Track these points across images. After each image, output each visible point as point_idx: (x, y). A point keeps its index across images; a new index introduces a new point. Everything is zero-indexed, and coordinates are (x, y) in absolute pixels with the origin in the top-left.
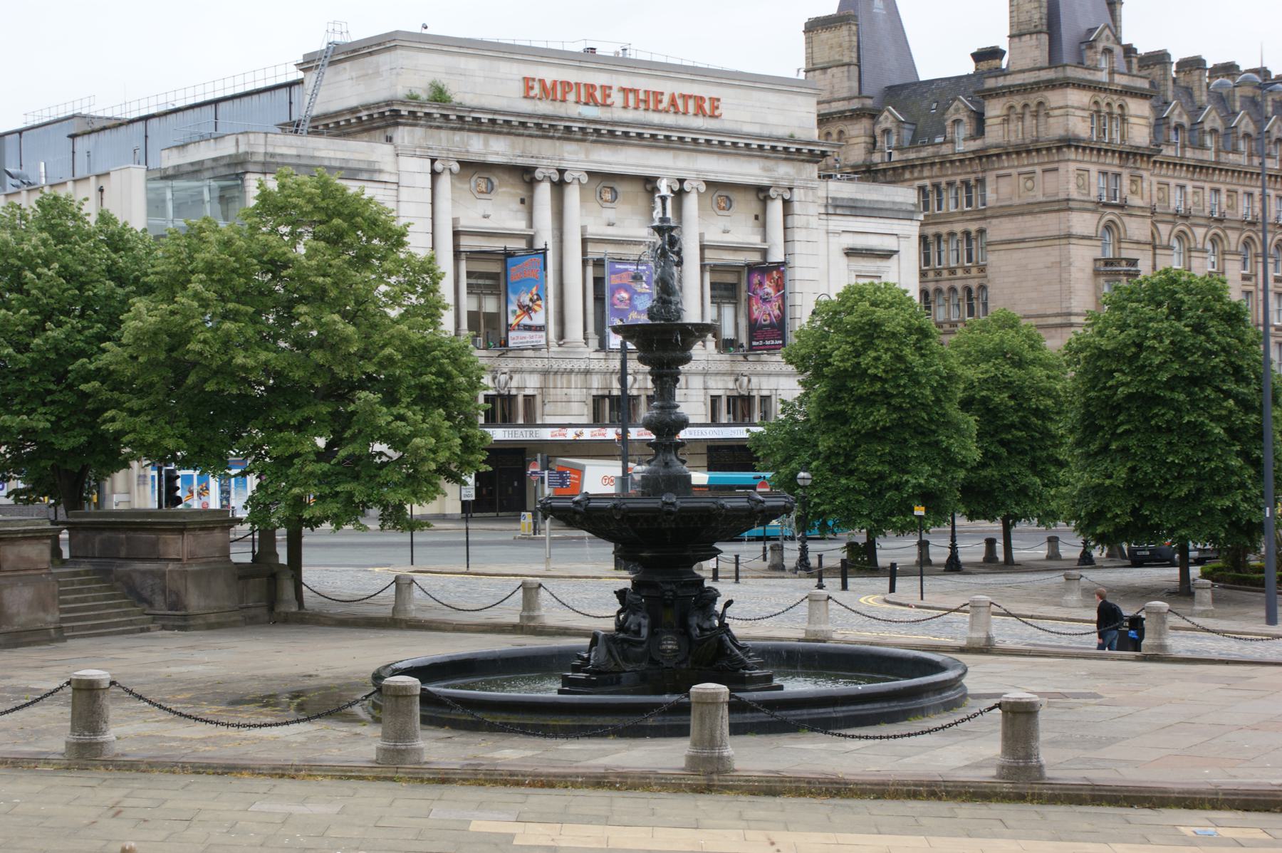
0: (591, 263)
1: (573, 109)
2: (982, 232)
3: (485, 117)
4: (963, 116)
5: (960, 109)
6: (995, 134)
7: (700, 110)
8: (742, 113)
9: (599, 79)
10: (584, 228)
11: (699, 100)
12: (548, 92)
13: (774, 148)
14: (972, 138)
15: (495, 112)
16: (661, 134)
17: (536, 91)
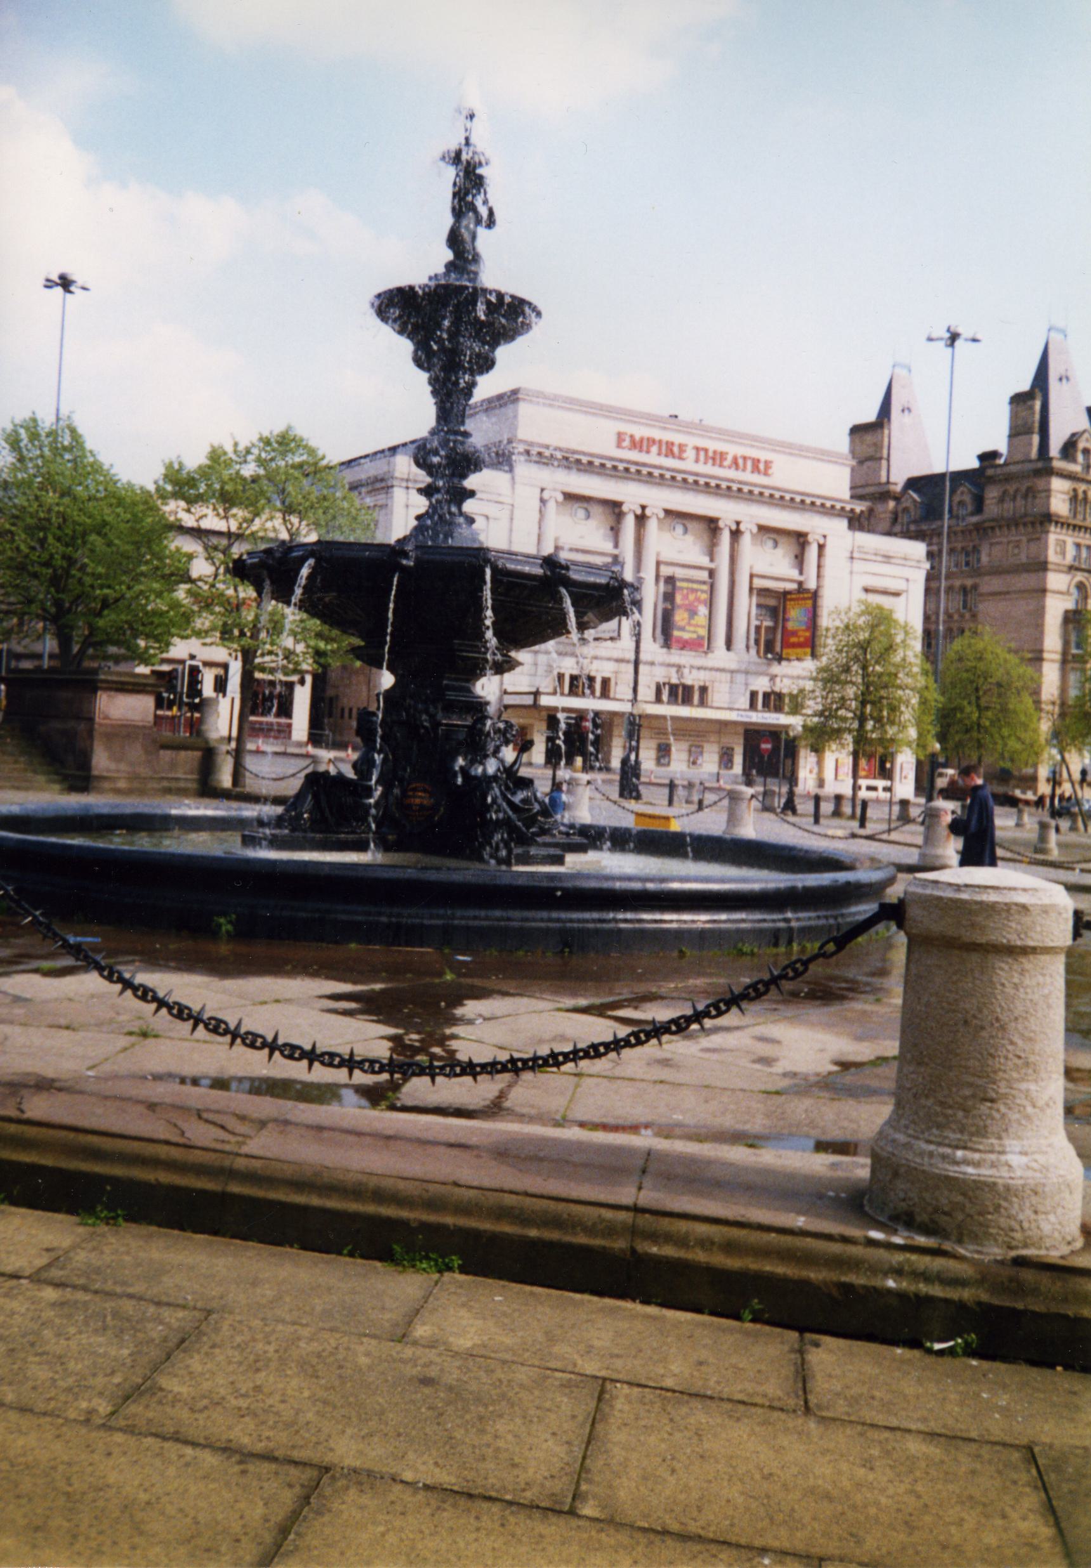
1: (653, 458)
2: (975, 587)
3: (585, 459)
4: (967, 498)
5: (965, 494)
6: (992, 508)
7: (756, 468)
8: (789, 475)
9: (677, 438)
10: (658, 554)
11: (756, 462)
12: (637, 444)
14: (972, 514)
16: (713, 483)
17: (626, 443)
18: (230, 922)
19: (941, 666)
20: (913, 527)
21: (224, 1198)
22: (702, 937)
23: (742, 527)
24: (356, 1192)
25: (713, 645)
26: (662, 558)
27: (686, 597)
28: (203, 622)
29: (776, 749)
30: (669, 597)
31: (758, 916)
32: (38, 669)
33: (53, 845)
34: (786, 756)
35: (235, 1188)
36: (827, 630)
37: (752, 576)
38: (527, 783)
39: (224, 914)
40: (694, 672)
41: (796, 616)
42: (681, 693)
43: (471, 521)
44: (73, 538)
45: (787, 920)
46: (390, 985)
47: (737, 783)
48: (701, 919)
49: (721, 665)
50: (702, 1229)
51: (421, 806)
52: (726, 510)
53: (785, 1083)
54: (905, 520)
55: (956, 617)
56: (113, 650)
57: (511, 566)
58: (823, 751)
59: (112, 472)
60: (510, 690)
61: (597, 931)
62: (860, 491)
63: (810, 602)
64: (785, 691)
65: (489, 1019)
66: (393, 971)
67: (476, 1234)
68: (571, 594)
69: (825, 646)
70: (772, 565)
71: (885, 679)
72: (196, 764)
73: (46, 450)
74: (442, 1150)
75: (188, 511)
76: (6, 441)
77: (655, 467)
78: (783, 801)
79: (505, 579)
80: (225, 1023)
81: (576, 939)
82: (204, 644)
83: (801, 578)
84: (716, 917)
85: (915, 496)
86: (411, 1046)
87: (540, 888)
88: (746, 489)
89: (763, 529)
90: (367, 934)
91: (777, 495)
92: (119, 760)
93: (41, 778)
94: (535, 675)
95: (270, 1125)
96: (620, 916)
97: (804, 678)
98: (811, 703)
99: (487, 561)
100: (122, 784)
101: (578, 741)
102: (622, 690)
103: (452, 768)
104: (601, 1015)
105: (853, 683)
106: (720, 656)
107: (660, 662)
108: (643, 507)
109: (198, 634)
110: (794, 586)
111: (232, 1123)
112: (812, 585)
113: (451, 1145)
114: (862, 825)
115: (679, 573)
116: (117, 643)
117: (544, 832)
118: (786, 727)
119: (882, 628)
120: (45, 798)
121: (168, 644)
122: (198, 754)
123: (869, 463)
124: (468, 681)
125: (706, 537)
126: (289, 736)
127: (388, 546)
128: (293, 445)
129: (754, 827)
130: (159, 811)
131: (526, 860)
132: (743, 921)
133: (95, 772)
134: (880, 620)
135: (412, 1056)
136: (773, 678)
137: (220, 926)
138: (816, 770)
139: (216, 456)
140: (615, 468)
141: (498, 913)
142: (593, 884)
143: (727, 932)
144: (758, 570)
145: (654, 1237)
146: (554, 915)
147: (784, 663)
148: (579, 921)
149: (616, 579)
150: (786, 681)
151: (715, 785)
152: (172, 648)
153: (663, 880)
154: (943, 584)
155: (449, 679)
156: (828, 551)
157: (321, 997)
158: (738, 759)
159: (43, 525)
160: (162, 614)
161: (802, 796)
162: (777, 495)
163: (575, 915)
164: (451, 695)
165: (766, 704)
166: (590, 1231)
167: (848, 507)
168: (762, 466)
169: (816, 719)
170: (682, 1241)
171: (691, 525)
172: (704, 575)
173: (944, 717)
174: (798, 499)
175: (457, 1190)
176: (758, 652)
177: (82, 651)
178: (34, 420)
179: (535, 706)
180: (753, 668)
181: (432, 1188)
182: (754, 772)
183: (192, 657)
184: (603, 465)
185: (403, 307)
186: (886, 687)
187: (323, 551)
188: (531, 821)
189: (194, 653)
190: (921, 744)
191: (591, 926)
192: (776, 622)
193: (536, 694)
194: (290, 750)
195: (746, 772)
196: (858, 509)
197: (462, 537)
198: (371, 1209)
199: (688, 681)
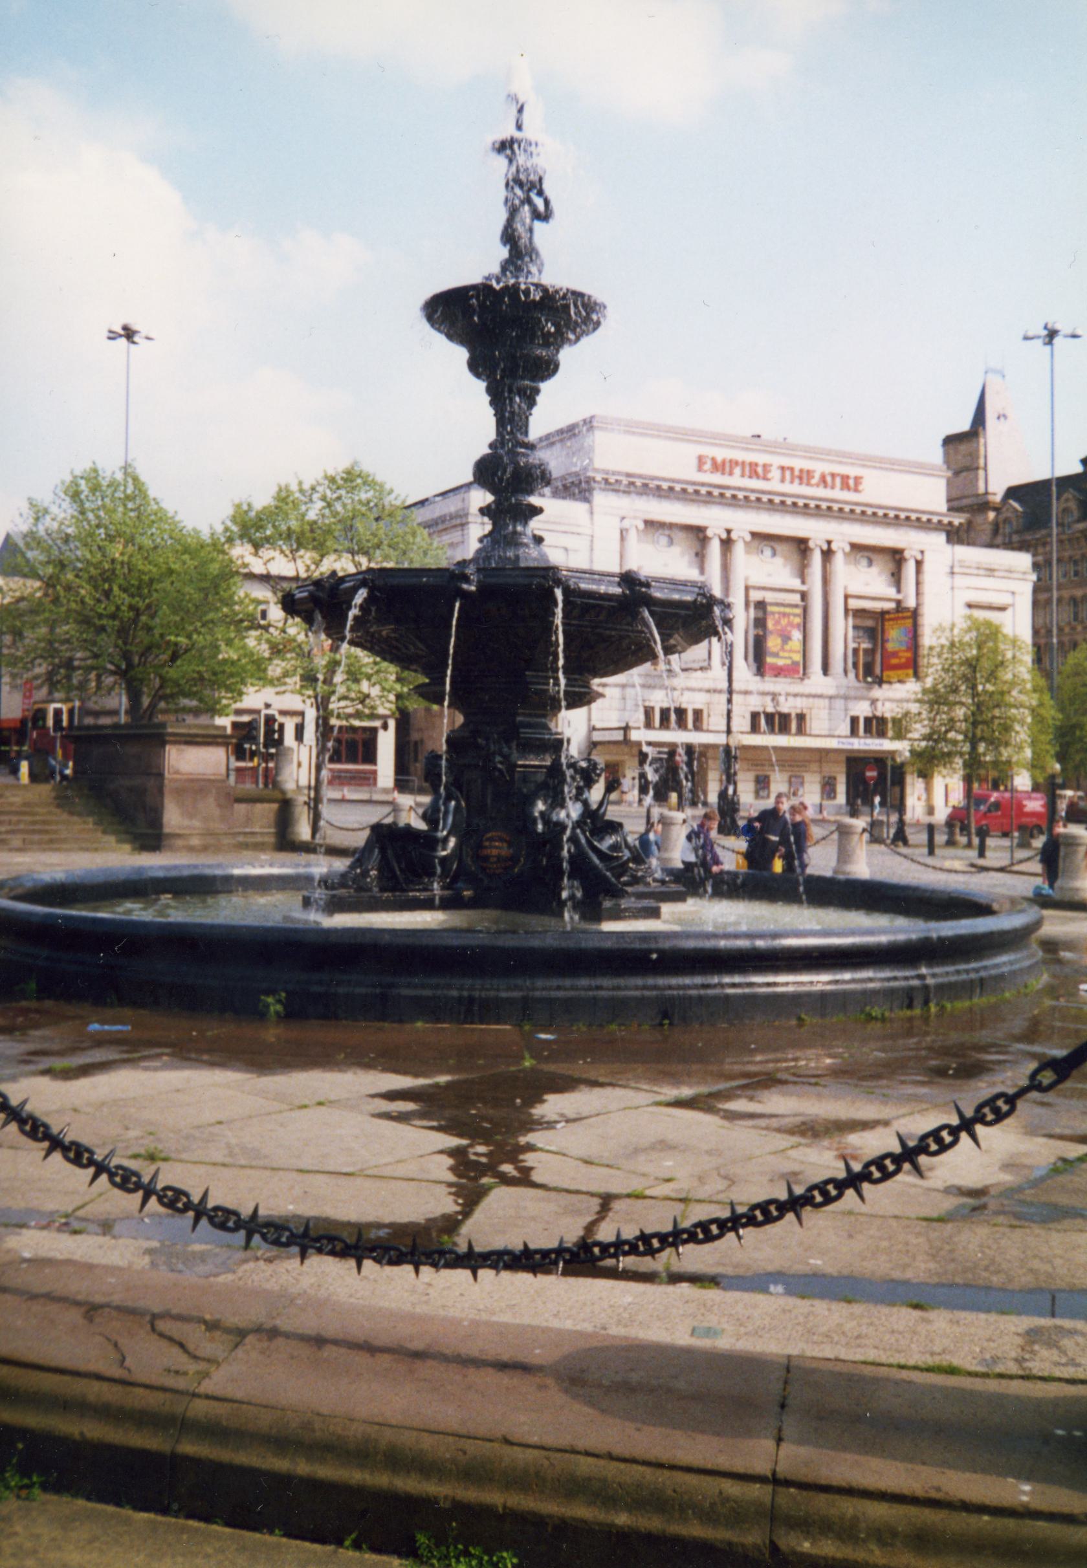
0: (851, 613)
1: (736, 480)
3: (665, 485)
7: (845, 486)
8: (880, 490)
9: (761, 459)
10: (746, 579)
11: (845, 478)
12: (718, 467)
13: (908, 518)
14: (1079, 521)
15: (673, 481)
16: (801, 502)
17: (708, 466)
18: (279, 1001)
19: (1057, 679)
20: (1015, 538)
21: (175, 1463)
22: (822, 1001)
23: (834, 546)
24: (361, 1453)
25: (809, 671)
26: (750, 583)
27: (777, 622)
28: (276, 669)
29: (882, 777)
30: (760, 623)
31: (887, 973)
32: (116, 726)
33: (84, 920)
34: (893, 784)
35: (189, 1448)
36: (931, 648)
37: (846, 597)
38: (615, 827)
39: (268, 992)
40: (791, 699)
41: (895, 637)
42: (779, 722)
43: (539, 540)
44: (139, 588)
45: (921, 977)
46: (456, 1077)
47: (842, 814)
48: (819, 981)
49: (819, 691)
50: (878, 1511)
51: (499, 857)
52: (815, 530)
53: (949, 1203)
54: (1007, 530)
55: (1067, 630)
56: (185, 702)
57: (583, 586)
58: (932, 777)
59: (177, 518)
60: (598, 726)
61: (700, 998)
62: (956, 504)
63: (909, 622)
64: (888, 715)
65: (575, 1120)
66: (464, 1056)
67: (538, 1521)
68: (652, 613)
69: (929, 665)
70: (869, 584)
71: (996, 697)
72: (272, 816)
73: (107, 500)
74: (490, 1377)
75: (256, 554)
76: (66, 493)
77: (739, 489)
78: (892, 831)
79: (579, 601)
80: (186, 1194)
81: (678, 1017)
82: (277, 693)
83: (899, 597)
84: (838, 977)
85: (1016, 505)
86: (477, 1163)
87: (633, 950)
88: (836, 507)
89: (856, 548)
90: (434, 1010)
91: (869, 511)
92: (191, 816)
93: (112, 839)
94: (624, 709)
95: (250, 1339)
96: (727, 980)
97: (908, 701)
98: (918, 726)
99: (558, 582)
100: (195, 841)
101: (673, 776)
102: (716, 721)
103: (532, 813)
104: (710, 1110)
105: (963, 704)
106: (817, 681)
107: (755, 692)
108: (729, 531)
109: (271, 682)
110: (892, 605)
111: (195, 1335)
112: (911, 603)
113: (503, 1366)
114: (982, 854)
115: (769, 597)
116: (187, 695)
117: (636, 880)
118: (893, 754)
119: (990, 644)
120: (117, 859)
121: (241, 694)
122: (275, 806)
123: (964, 474)
124: (544, 716)
125: (796, 557)
126: (375, 783)
127: (446, 570)
128: (359, 481)
129: (867, 863)
130: (218, 872)
131: (617, 915)
132: (871, 980)
133: (166, 830)
134: (988, 636)
135: (475, 1179)
136: (874, 702)
137: (267, 1006)
138: (924, 797)
139: (283, 498)
140: (697, 492)
141: (584, 982)
142: (691, 944)
143: (853, 993)
144: (852, 590)
145: (805, 1525)
146: (650, 981)
147: (885, 686)
148: (679, 987)
149: (704, 595)
150: (888, 705)
151: (820, 817)
152: (244, 697)
153: (775, 935)
154: (1055, 594)
155: (524, 715)
156: (927, 567)
157: (373, 1096)
158: (841, 789)
159: (108, 576)
160: (233, 663)
161: (911, 825)
162: (869, 511)
163: (674, 981)
164: (526, 733)
165: (868, 730)
166: (709, 1515)
167: (946, 520)
168: (851, 482)
169: (923, 744)
170: (847, 1532)
171: (780, 547)
172: (796, 599)
173: (1063, 735)
174: (892, 514)
175: (508, 1450)
176: (857, 676)
177: (153, 706)
178: (95, 471)
179: (626, 741)
180: (852, 693)
181: (471, 1447)
182: (859, 802)
183: (268, 706)
184: (684, 491)
185: (452, 311)
186: (998, 706)
187: (374, 580)
188: (622, 869)
189: (269, 702)
190: (1035, 765)
191: (693, 992)
192: (875, 645)
193: (626, 729)
194: (376, 797)
195: (851, 801)
196: (956, 522)
197: (530, 556)
198: (382, 1480)
199: (784, 709)
